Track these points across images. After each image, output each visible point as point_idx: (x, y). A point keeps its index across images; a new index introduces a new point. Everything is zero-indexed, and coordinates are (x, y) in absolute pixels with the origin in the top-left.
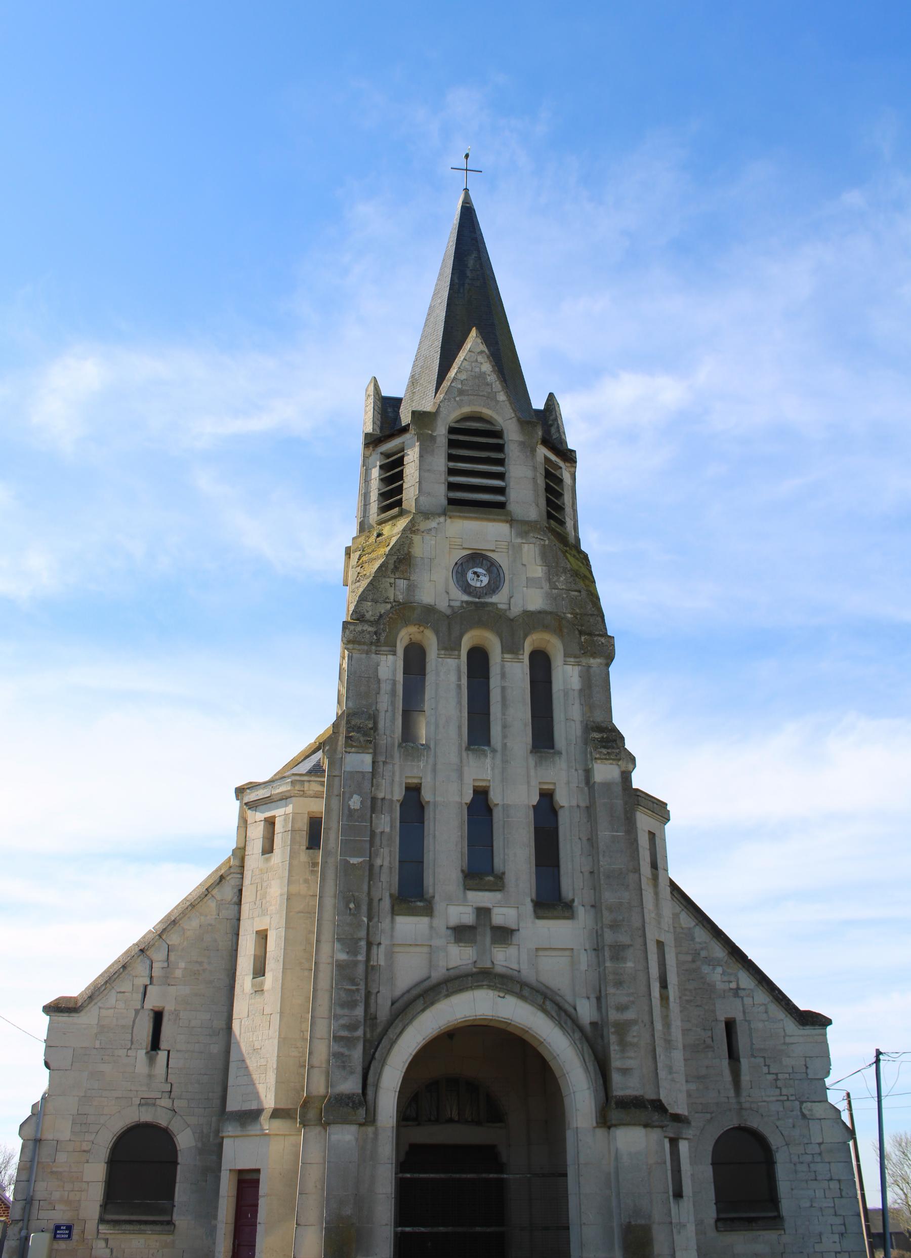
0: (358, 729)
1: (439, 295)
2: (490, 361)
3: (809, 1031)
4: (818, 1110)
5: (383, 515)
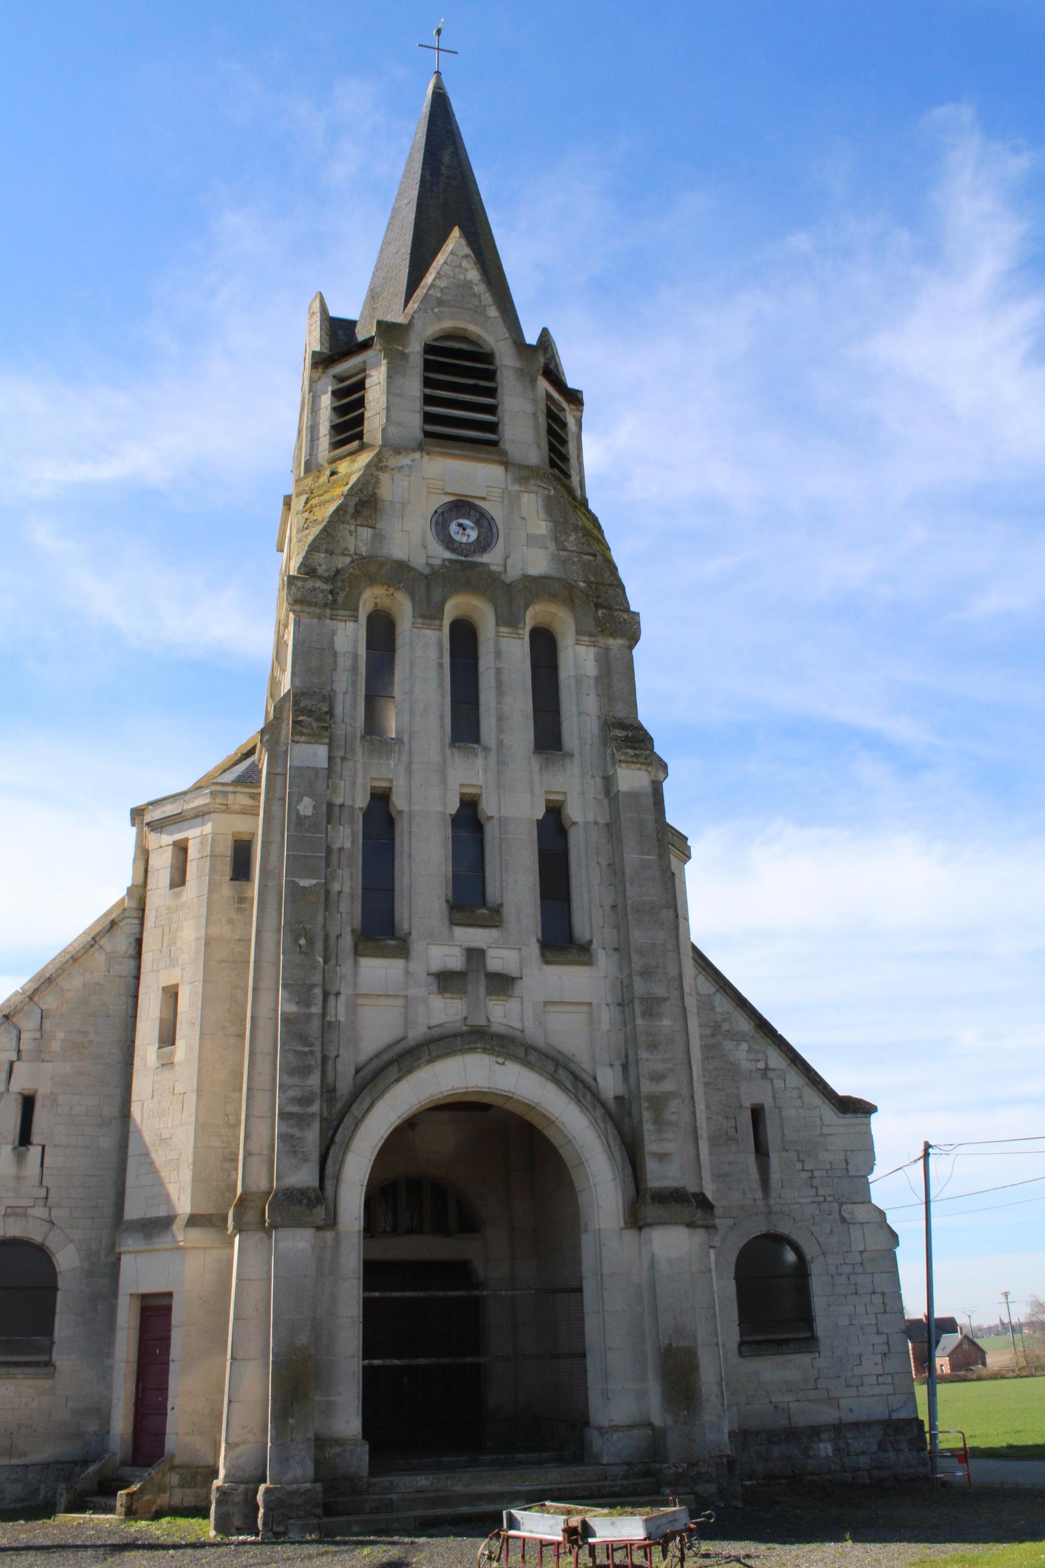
0: (310, 713)
1: (406, 194)
2: (478, 269)
3: (849, 1119)
4: (860, 1213)
5: (338, 451)
